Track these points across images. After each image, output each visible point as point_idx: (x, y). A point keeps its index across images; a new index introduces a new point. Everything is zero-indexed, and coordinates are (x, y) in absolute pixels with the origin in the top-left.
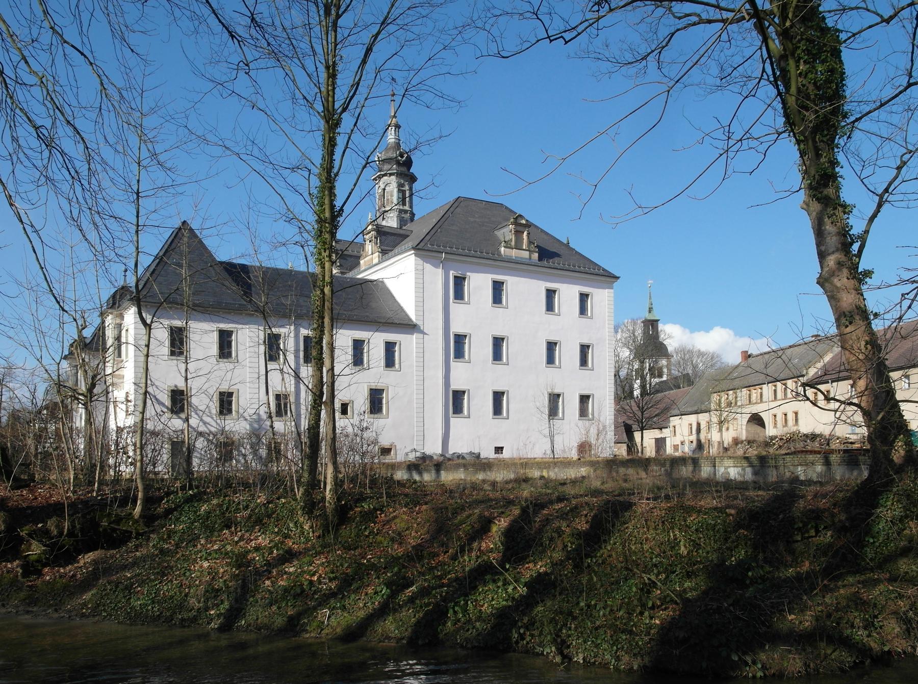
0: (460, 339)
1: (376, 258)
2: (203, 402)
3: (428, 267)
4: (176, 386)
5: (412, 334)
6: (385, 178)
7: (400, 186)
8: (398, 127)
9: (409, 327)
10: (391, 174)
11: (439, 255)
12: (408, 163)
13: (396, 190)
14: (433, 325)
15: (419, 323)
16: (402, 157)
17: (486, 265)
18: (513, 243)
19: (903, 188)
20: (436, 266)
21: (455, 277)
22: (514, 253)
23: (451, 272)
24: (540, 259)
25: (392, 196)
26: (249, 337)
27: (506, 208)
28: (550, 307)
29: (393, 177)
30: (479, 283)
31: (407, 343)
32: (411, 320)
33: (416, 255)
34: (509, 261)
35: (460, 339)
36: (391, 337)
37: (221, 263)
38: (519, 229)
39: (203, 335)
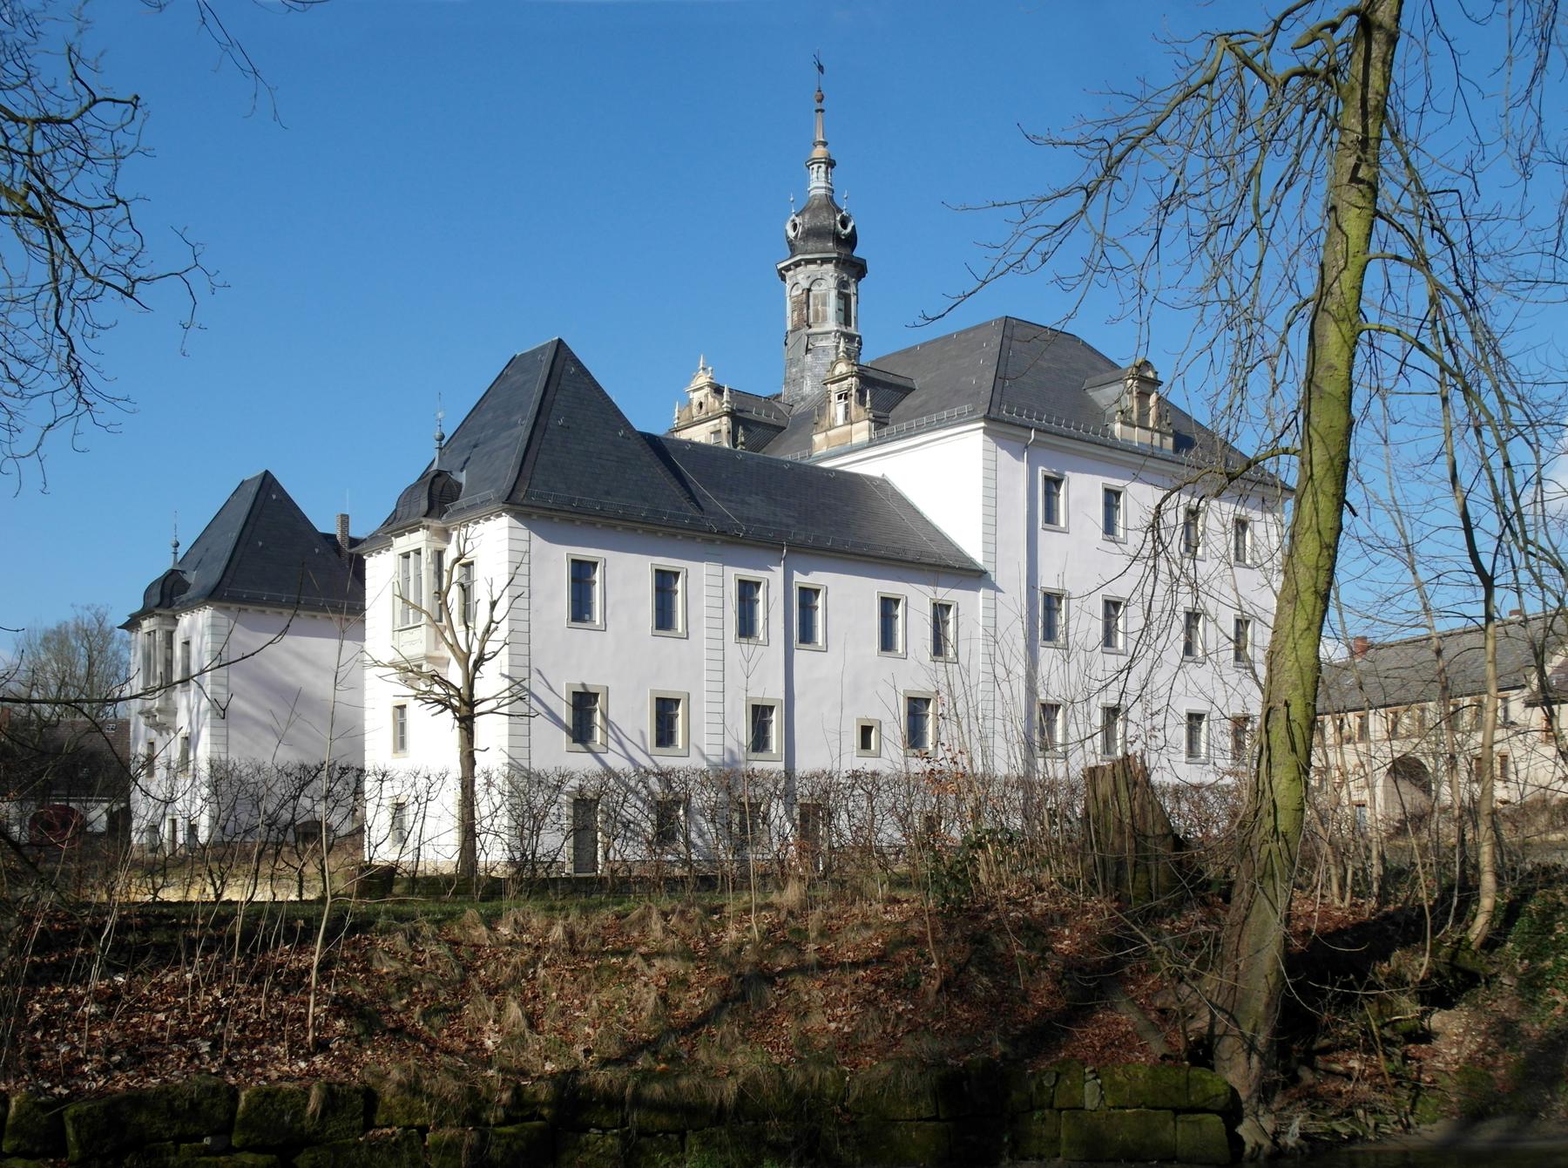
0: (1052, 601)
1: (862, 431)
2: (630, 715)
3: (1004, 456)
4: (583, 685)
5: (977, 589)
6: (812, 267)
7: (842, 285)
8: (830, 164)
9: (971, 575)
10: (824, 261)
11: (1023, 433)
12: (851, 241)
13: (833, 294)
14: (1010, 574)
15: (989, 568)
16: (845, 226)
17: (1081, 454)
18: (1135, 416)
19: (1162, 108)
20: (1018, 457)
21: (1047, 479)
22: (1137, 436)
23: (1040, 469)
24: (1177, 449)
25: (824, 304)
26: (707, 584)
27: (1084, 344)
28: (664, 619)
29: (830, 267)
30: (1083, 491)
31: (970, 605)
32: (974, 563)
33: (986, 431)
34: (1127, 448)
35: (1052, 601)
36: (945, 594)
37: (643, 435)
38: (1146, 388)
39: (626, 574)
